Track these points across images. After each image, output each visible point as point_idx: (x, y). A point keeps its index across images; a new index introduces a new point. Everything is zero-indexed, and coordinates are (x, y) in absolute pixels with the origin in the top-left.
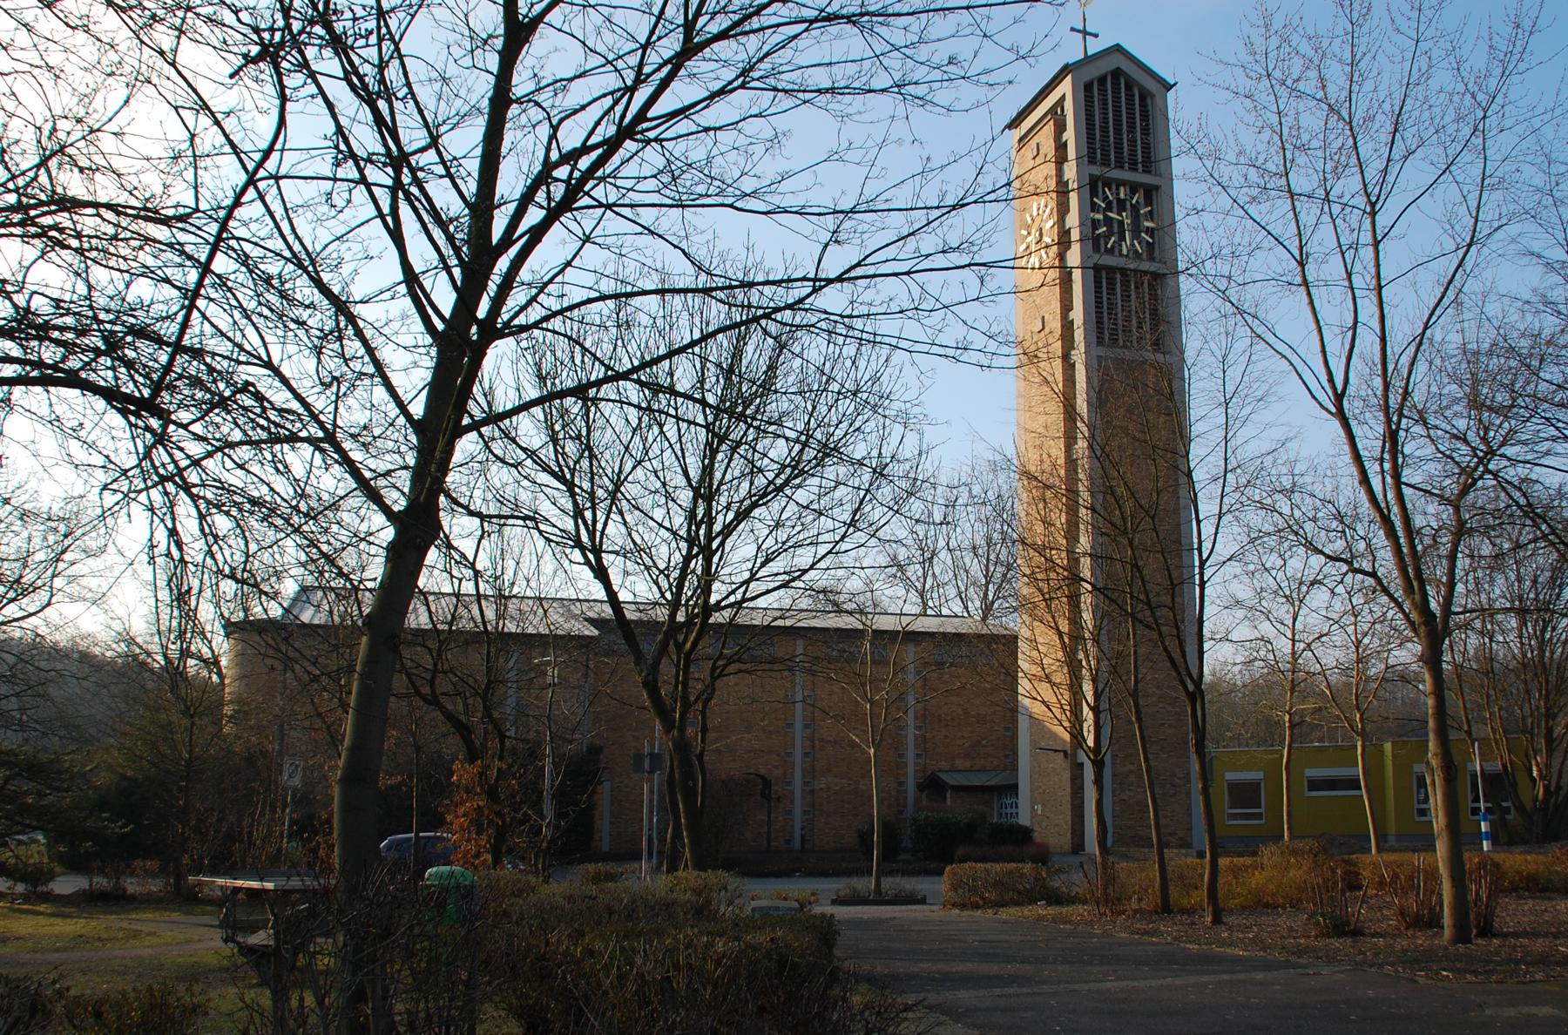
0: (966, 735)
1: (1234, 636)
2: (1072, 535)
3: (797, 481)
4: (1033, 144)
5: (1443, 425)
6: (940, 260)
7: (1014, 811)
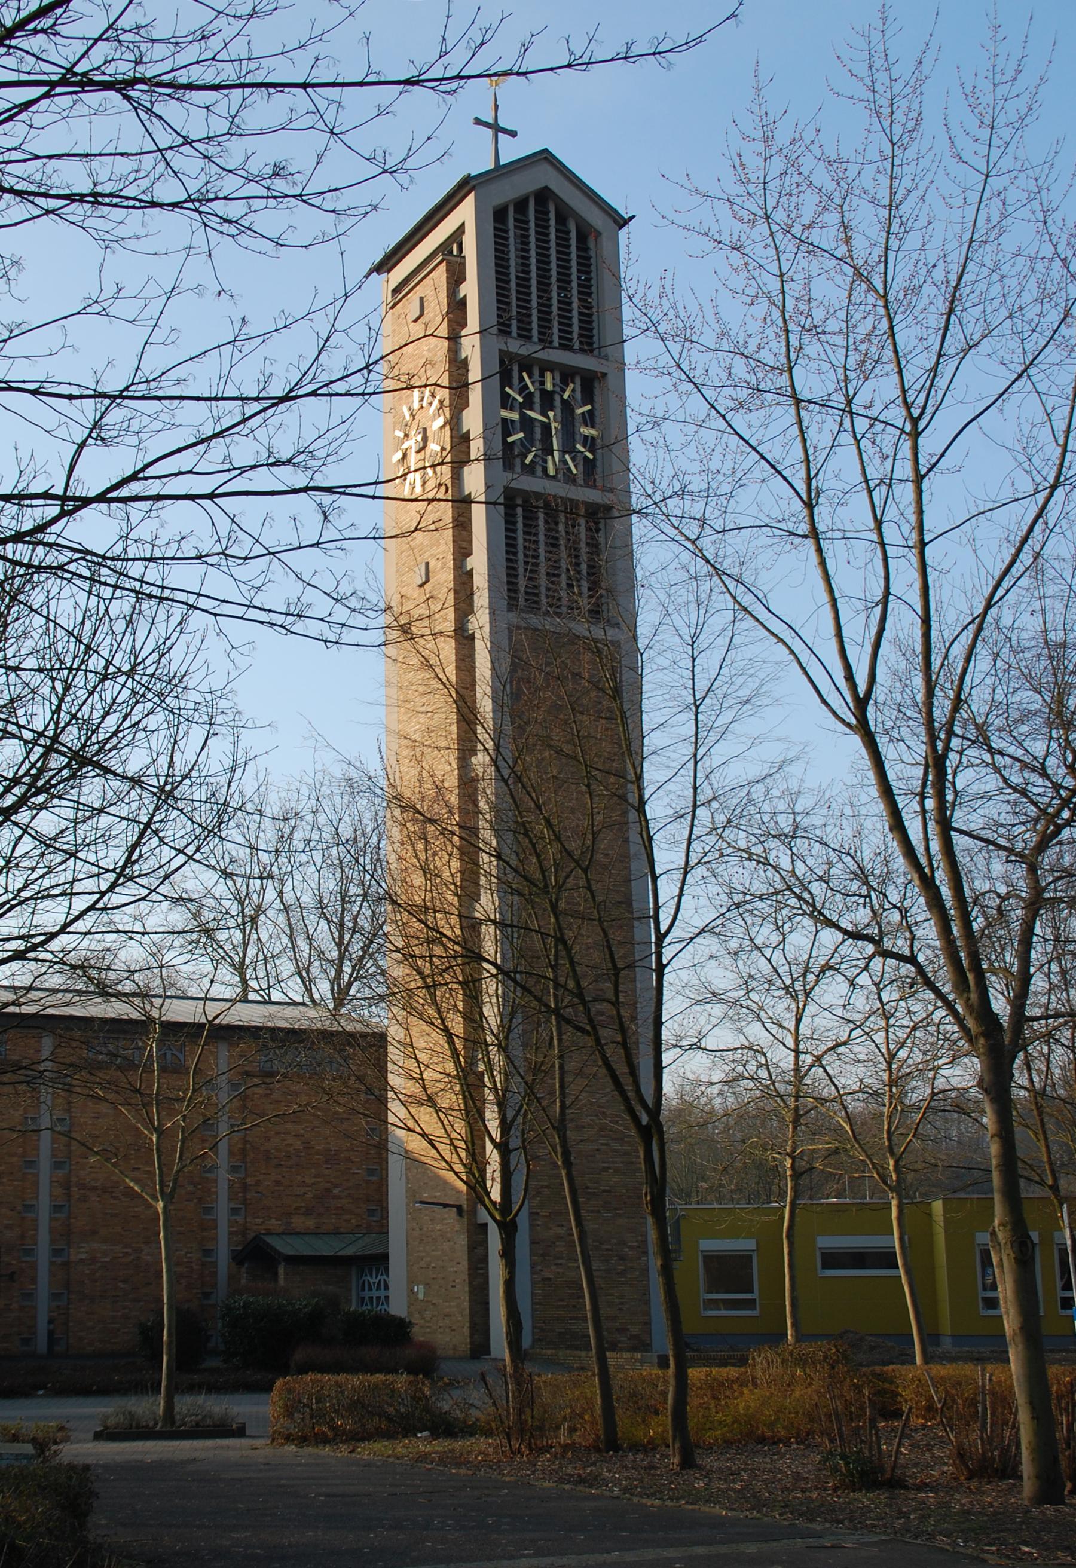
0: (309, 1181)
1: (709, 1043)
2: (469, 893)
3: (41, 799)
4: (414, 298)
5: (1012, 750)
6: (261, 480)
7: (382, 1293)
